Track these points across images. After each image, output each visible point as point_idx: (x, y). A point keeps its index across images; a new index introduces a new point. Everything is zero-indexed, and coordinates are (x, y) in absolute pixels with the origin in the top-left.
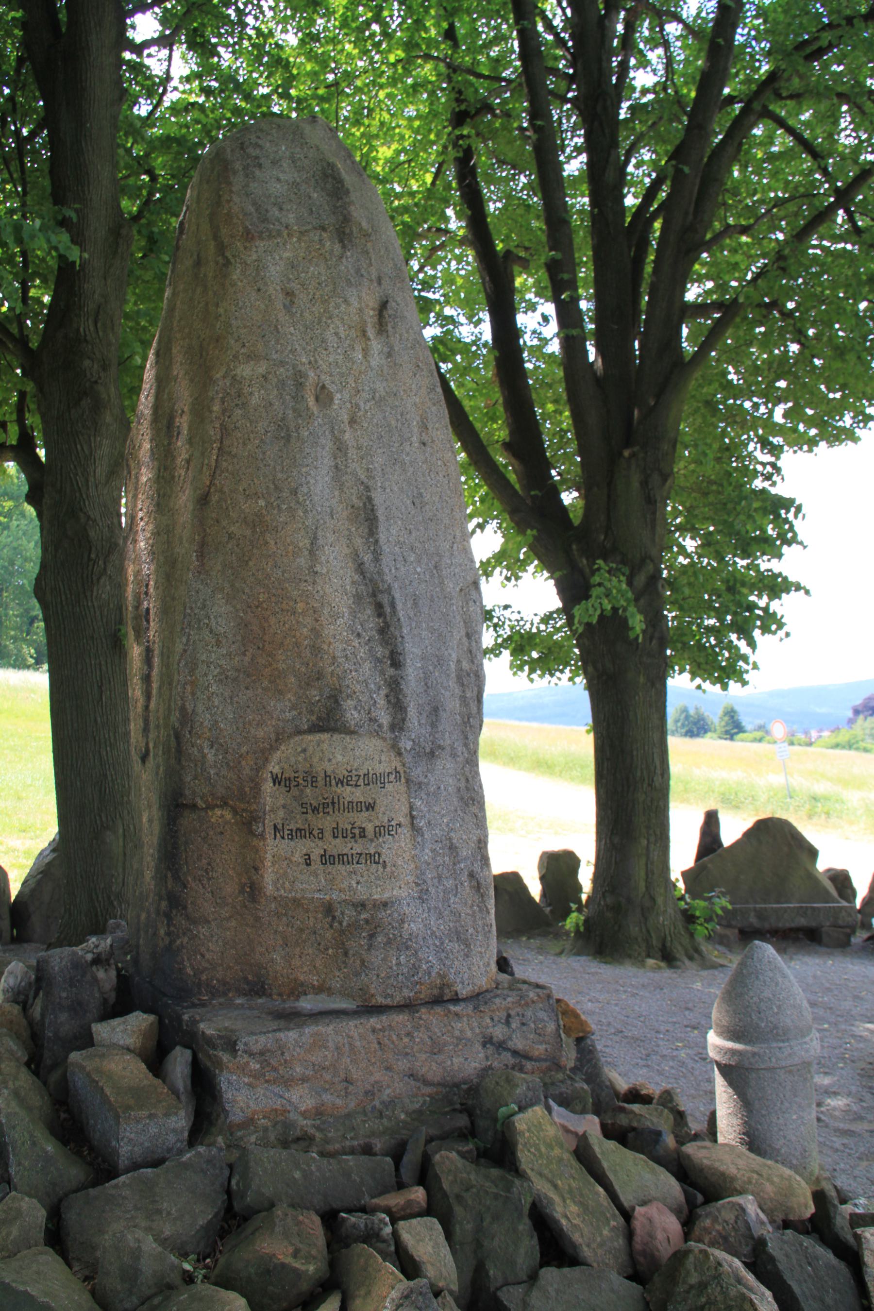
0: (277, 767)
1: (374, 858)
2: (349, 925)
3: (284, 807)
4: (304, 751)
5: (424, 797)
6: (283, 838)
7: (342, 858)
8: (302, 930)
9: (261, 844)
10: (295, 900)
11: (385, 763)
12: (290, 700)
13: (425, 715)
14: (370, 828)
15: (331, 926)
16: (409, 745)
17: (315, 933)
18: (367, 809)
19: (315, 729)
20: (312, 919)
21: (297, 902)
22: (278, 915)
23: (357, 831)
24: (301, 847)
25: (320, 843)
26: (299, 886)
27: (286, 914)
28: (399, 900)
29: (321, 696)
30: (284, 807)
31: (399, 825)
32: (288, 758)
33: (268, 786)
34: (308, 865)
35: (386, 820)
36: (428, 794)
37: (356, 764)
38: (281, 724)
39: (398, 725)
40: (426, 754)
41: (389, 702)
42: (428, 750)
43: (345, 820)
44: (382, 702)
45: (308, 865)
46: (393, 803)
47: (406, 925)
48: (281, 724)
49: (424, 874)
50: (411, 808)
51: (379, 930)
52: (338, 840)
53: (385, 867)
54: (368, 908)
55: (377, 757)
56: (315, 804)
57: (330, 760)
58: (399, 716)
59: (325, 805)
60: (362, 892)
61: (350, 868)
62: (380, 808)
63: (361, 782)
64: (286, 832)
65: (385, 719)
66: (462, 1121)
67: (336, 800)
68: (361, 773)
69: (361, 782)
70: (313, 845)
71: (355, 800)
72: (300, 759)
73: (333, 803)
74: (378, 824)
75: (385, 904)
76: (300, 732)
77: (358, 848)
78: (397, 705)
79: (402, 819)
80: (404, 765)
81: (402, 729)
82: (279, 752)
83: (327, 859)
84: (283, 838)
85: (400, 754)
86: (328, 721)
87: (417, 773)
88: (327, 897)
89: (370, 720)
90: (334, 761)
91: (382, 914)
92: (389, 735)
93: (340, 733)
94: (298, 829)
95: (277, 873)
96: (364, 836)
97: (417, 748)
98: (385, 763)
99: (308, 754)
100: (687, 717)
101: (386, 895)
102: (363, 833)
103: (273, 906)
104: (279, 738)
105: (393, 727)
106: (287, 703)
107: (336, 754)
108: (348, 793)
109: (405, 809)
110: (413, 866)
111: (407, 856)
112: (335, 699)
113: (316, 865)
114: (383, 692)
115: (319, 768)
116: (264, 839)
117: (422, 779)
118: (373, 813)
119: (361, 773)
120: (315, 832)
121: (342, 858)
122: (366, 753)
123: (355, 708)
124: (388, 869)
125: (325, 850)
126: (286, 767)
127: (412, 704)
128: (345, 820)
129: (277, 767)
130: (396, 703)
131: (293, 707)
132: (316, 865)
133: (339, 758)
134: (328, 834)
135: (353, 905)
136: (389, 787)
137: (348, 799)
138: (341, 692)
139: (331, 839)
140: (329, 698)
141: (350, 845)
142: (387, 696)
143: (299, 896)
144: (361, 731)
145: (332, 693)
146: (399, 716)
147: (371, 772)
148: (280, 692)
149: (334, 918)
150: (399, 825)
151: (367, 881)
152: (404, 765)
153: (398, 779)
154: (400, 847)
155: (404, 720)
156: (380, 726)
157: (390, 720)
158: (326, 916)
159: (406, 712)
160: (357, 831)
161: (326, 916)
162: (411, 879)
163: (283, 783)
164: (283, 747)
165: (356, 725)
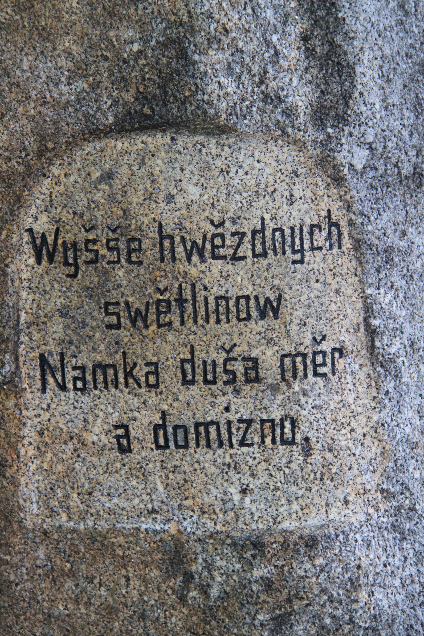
0: (44, 218)
1: (282, 432)
2: (225, 596)
3: (63, 312)
4: (108, 177)
5: (400, 283)
6: (63, 388)
7: (204, 433)
8: (111, 611)
9: (11, 403)
10: (93, 537)
11: (303, 204)
12: (69, 53)
13: (398, 83)
14: (269, 358)
15: (182, 599)
16: (360, 157)
17: (143, 617)
18: (263, 315)
19: (132, 123)
20: (135, 583)
21: (98, 542)
22: (54, 576)
23: (239, 367)
24: (107, 408)
25: (152, 398)
26: (102, 502)
27: (72, 574)
28: (344, 534)
29: (145, 40)
30: (63, 312)
31: (340, 351)
32: (70, 197)
33: (24, 264)
34: (125, 450)
35: (308, 341)
36: (409, 277)
37: (233, 208)
38: (49, 113)
39: (334, 110)
40: (401, 179)
41: (310, 53)
42: (407, 169)
43: (210, 342)
44: (292, 54)
45: (125, 450)
46: (324, 298)
47: (363, 595)
48: (49, 113)
49: (400, 468)
50: (368, 310)
51: (297, 605)
52: (194, 390)
53: (307, 451)
54: (270, 551)
55: (282, 189)
56: (137, 303)
57: (170, 198)
58: (335, 88)
59: (162, 307)
60: (254, 515)
61: (223, 455)
62: (294, 312)
63: (245, 249)
64: (70, 374)
65: (301, 95)
66: (319, 338)
67: (187, 294)
68: (247, 228)
69: (245, 249)
70: (135, 402)
71: (233, 292)
72: (98, 196)
73: (181, 301)
74: (288, 348)
75: (311, 543)
76: (96, 133)
77: (242, 407)
78: (331, 61)
79: (346, 338)
80: (349, 208)
81: (342, 119)
82: (47, 182)
83: (169, 435)
84: (63, 388)
85: (338, 180)
86: (164, 101)
87: (382, 225)
88: (172, 527)
89: (266, 97)
90: (179, 199)
91: (303, 567)
92: (312, 134)
93: (194, 132)
94: (97, 366)
95: (49, 472)
96: (258, 379)
97: (380, 164)
98: (303, 204)
99: (117, 184)
100: (338, 184)
101: (313, 521)
102: (253, 372)
103: (41, 553)
104: (48, 148)
105: (321, 115)
106: (62, 62)
107: (184, 183)
108: (215, 277)
109: (354, 314)
110: (375, 450)
111: (360, 425)
112: (178, 47)
113: (144, 451)
114: (295, 30)
115: (145, 218)
116: (18, 393)
117: (393, 239)
118: (276, 324)
119: (247, 228)
120: (140, 372)
121: (204, 433)
122: (256, 178)
123: (229, 70)
124: (316, 457)
125: (164, 415)
126: (66, 216)
127: (366, 56)
128: (210, 342)
129: (44, 218)
130: (328, 57)
131: (79, 71)
132: (144, 451)
133: (194, 192)
134: (170, 377)
135: (234, 544)
136: (315, 261)
137: (216, 291)
138: (193, 31)
139: (177, 386)
140: (163, 45)
141: (222, 401)
142: (305, 38)
143: (103, 526)
144: (241, 127)
145: (172, 33)
146: (335, 88)
147: (270, 225)
148: (45, 34)
149: (189, 577)
150: (340, 351)
151: (265, 487)
152: (349, 208)
153: (335, 240)
154: (345, 405)
155: (346, 97)
156: (289, 113)
157: (313, 97)
158: (169, 575)
159: (352, 75)
160: (239, 367)
161: (169, 575)
162: (371, 480)
163: (59, 257)
164: (55, 170)
165: (232, 111)
